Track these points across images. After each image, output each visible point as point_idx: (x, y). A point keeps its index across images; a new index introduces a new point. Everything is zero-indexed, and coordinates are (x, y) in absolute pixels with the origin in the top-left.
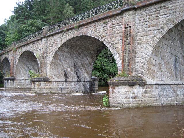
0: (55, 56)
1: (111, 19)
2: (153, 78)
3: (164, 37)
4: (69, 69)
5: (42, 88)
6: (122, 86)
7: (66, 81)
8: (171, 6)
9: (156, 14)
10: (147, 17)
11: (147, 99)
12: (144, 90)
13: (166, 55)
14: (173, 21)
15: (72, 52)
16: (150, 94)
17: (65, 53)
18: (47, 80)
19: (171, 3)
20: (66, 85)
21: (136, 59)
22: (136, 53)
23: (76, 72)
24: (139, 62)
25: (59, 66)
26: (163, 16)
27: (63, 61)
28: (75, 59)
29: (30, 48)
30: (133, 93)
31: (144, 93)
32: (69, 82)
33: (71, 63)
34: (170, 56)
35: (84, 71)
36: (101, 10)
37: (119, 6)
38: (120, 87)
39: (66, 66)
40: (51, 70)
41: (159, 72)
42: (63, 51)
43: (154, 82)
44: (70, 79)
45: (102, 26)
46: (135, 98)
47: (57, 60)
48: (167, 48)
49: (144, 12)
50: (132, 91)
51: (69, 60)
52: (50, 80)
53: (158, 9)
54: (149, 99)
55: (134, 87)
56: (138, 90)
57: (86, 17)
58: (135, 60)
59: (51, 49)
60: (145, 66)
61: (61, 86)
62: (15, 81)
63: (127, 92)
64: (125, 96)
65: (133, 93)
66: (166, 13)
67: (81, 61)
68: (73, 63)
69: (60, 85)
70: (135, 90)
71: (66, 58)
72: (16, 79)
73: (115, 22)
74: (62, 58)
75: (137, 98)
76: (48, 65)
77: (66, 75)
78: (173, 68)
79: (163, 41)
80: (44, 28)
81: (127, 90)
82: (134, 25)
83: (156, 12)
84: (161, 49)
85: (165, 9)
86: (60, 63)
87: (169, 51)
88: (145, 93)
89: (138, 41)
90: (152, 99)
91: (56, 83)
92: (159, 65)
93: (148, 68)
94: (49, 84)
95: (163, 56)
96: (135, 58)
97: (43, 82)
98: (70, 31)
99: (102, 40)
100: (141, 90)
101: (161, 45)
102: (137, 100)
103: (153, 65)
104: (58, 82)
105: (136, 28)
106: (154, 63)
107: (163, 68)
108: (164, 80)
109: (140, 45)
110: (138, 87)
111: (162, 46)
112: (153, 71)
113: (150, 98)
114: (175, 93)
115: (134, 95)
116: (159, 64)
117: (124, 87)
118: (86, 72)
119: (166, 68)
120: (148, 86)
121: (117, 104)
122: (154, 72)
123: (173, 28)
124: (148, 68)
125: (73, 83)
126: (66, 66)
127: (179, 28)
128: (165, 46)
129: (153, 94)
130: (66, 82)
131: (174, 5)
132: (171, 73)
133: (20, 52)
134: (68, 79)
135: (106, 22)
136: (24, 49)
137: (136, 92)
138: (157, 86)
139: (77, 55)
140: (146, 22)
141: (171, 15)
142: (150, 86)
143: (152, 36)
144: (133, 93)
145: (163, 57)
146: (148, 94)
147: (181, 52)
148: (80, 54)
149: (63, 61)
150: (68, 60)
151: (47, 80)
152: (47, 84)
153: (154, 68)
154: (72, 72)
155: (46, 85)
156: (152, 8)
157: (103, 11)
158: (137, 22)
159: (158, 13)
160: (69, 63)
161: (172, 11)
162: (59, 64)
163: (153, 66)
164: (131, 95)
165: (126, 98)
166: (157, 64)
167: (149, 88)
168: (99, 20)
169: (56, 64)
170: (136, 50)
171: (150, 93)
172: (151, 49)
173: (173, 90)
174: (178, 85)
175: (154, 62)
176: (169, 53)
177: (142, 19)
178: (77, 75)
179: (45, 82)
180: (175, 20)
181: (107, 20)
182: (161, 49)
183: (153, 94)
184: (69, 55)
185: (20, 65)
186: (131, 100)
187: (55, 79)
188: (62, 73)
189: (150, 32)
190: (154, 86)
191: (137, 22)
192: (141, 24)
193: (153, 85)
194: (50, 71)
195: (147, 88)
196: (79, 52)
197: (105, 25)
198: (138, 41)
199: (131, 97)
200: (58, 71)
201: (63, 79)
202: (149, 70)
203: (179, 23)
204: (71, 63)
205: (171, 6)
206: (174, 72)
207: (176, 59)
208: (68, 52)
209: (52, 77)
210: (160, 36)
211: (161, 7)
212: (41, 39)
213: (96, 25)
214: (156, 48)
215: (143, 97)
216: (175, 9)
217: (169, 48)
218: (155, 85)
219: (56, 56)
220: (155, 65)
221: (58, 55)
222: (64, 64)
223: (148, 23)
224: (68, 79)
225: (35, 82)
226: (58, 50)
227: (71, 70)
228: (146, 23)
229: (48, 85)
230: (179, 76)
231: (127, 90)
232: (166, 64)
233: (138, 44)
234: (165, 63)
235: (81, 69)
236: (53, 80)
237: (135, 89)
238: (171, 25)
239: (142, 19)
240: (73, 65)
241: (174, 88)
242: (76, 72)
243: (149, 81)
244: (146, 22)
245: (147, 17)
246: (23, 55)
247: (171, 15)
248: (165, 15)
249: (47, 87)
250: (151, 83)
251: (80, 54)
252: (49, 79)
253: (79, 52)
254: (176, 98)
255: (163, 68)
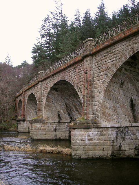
0: (47, 99)
1: (78, 65)
2: (109, 121)
3: (111, 81)
4: (62, 111)
5: (38, 129)
6: (78, 129)
7: (59, 122)
8: (114, 51)
9: (105, 59)
10: (100, 63)
11: (103, 141)
12: (100, 133)
13: (120, 98)
14: (116, 66)
15: (62, 94)
16: (106, 137)
17: (56, 96)
18: (42, 122)
19: (114, 48)
21: (94, 103)
22: (93, 97)
23: (69, 113)
24: (96, 106)
25: (53, 108)
26: (110, 61)
27: (55, 104)
28: (67, 101)
30: (89, 136)
31: (100, 136)
32: (63, 124)
33: (63, 105)
35: (76, 112)
36: (128, 24)
38: (76, 130)
39: (59, 108)
40: (46, 112)
41: (114, 115)
42: (53, 94)
43: (108, 125)
44: (63, 121)
45: (73, 72)
46: (90, 140)
48: (119, 91)
49: (98, 57)
50: (87, 133)
51: (61, 102)
52: (45, 122)
53: (106, 54)
54: (105, 141)
55: (90, 130)
56: (93, 133)
57: (104, 39)
58: (92, 104)
59: (45, 92)
60: (99, 110)
63: (82, 135)
64: (80, 138)
65: (89, 136)
66: (111, 58)
67: (72, 102)
68: (65, 105)
70: (91, 133)
72: (26, 120)
73: (80, 67)
75: (93, 141)
76: (43, 107)
77: (59, 116)
79: (112, 84)
80: (39, 73)
81: (83, 133)
82: (90, 71)
83: (105, 57)
84: (113, 92)
85: (110, 54)
86: (53, 105)
87: (122, 93)
88: (101, 135)
89: (95, 86)
90: (108, 142)
92: (115, 109)
93: (102, 111)
96: (92, 102)
97: (39, 124)
98: (55, 76)
99: (73, 85)
100: (97, 133)
101: (111, 89)
102: (92, 142)
103: (107, 108)
104: (52, 124)
105: (93, 73)
106: (108, 106)
109: (96, 89)
110: (93, 130)
111: (113, 89)
112: (108, 114)
113: (106, 140)
114: (134, 136)
115: (89, 138)
117: (80, 130)
118: (78, 113)
119: (122, 111)
120: (103, 129)
121: (75, 146)
122: (109, 115)
123: (117, 72)
124: (102, 111)
125: (66, 124)
127: (123, 71)
129: (110, 136)
130: (60, 123)
131: (116, 49)
133: (50, 83)
134: (62, 120)
136: (57, 79)
137: (91, 135)
138: (113, 129)
139: (68, 97)
140: (99, 67)
141: (114, 59)
142: (105, 129)
143: (103, 80)
144: (88, 136)
146: (104, 137)
147: (136, 94)
148: (70, 96)
149: (55, 104)
150: (60, 102)
151: (42, 122)
152: (42, 126)
153: (110, 112)
154: (65, 113)
156: (102, 53)
157: (110, 33)
158: (94, 67)
159: (106, 58)
160: (61, 105)
161: (115, 56)
162: (52, 106)
163: (108, 109)
164: (87, 138)
165: (82, 140)
166: (112, 107)
167: (105, 131)
169: (49, 106)
170: (93, 94)
171: (106, 136)
172: (103, 92)
173: (131, 132)
174: (137, 128)
175: (108, 105)
176: (123, 96)
177: (97, 64)
178: (70, 116)
179: (41, 124)
180: (117, 65)
181: (76, 66)
182: (113, 92)
183: (109, 136)
184: (60, 98)
185: (29, 107)
186: (87, 142)
187: (51, 121)
189: (102, 76)
190: (110, 129)
191: (94, 67)
192: (96, 69)
193: (109, 127)
194: (45, 113)
195: (102, 131)
196: (69, 94)
197: (75, 71)
198: (95, 86)
201: (57, 120)
202: (104, 113)
203: (120, 67)
204: (63, 105)
205: (114, 51)
208: (58, 94)
210: (108, 80)
211: (108, 52)
212: (37, 84)
213: (69, 70)
214: (107, 91)
215: (98, 139)
216: (117, 54)
217: (121, 91)
218: (110, 127)
219: (48, 100)
220: (110, 108)
221: (49, 98)
222: (57, 106)
223: (100, 68)
224: (62, 120)
225: (32, 124)
226: (48, 94)
227: (63, 112)
228: (100, 68)
229: (43, 127)
231: (83, 133)
233: (95, 88)
235: (73, 110)
236: (48, 121)
237: (90, 132)
238: (115, 70)
239: (97, 64)
240: (65, 107)
241: (133, 131)
242: (69, 113)
243: (104, 124)
244: (99, 67)
245: (100, 63)
246: (55, 88)
247: (114, 59)
248: (111, 59)
250: (106, 126)
251: (70, 96)
253: (69, 94)
254: (135, 140)
255: (119, 110)
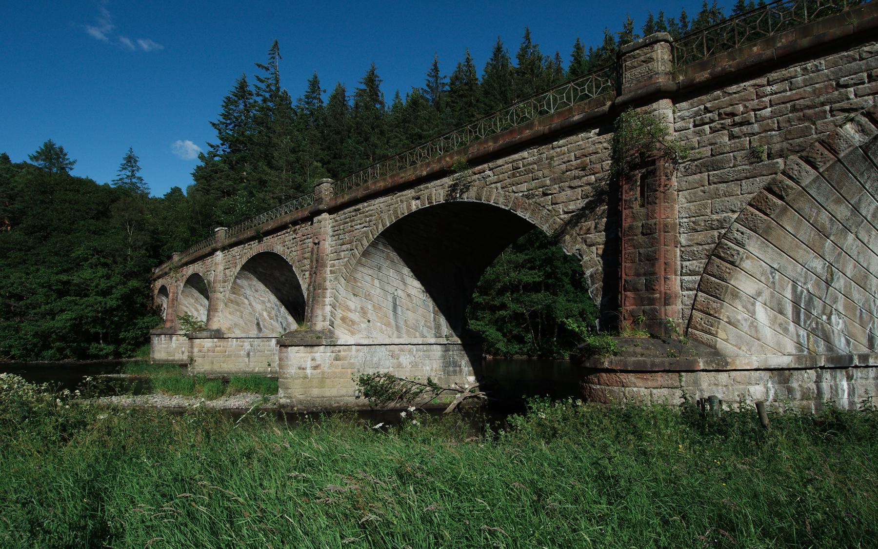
4: (265, 314)
20: (259, 346)
29: (277, 244)
34: (382, 294)
37: (512, 113)
39: (258, 307)
41: (363, 322)
46: (316, 368)
47: (239, 295)
48: (373, 280)
52: (225, 336)
53: (354, 214)
61: (249, 347)
62: (174, 338)
69: (247, 345)
71: (257, 291)
74: (248, 292)
78: (391, 314)
84: (361, 283)
86: (246, 301)
87: (378, 286)
88: (337, 359)
91: (237, 341)
92: (363, 312)
94: (221, 343)
95: (369, 295)
100: (329, 354)
102: (319, 371)
103: (350, 311)
107: (371, 315)
108: (373, 336)
111: (363, 277)
116: (362, 308)
119: (378, 316)
122: (353, 322)
126: (260, 308)
128: (368, 278)
129: (352, 361)
132: (388, 324)
135: (295, 230)
145: (368, 297)
149: (252, 299)
152: (218, 344)
154: (271, 318)
155: (216, 346)
159: (353, 220)
162: (243, 303)
165: (300, 368)
166: (359, 309)
168: (283, 227)
169: (238, 304)
179: (215, 340)
182: (361, 283)
188: (251, 322)
195: (339, 351)
199: (309, 366)
200: (242, 317)
206: (393, 323)
207: (395, 299)
209: (229, 329)
217: (377, 282)
221: (238, 285)
222: (254, 304)
227: (269, 316)
230: (404, 331)
232: (377, 308)
234: (374, 306)
236: (233, 336)
237: (317, 352)
245: (342, 227)
249: (219, 348)
250: (347, 341)
252: (223, 334)
